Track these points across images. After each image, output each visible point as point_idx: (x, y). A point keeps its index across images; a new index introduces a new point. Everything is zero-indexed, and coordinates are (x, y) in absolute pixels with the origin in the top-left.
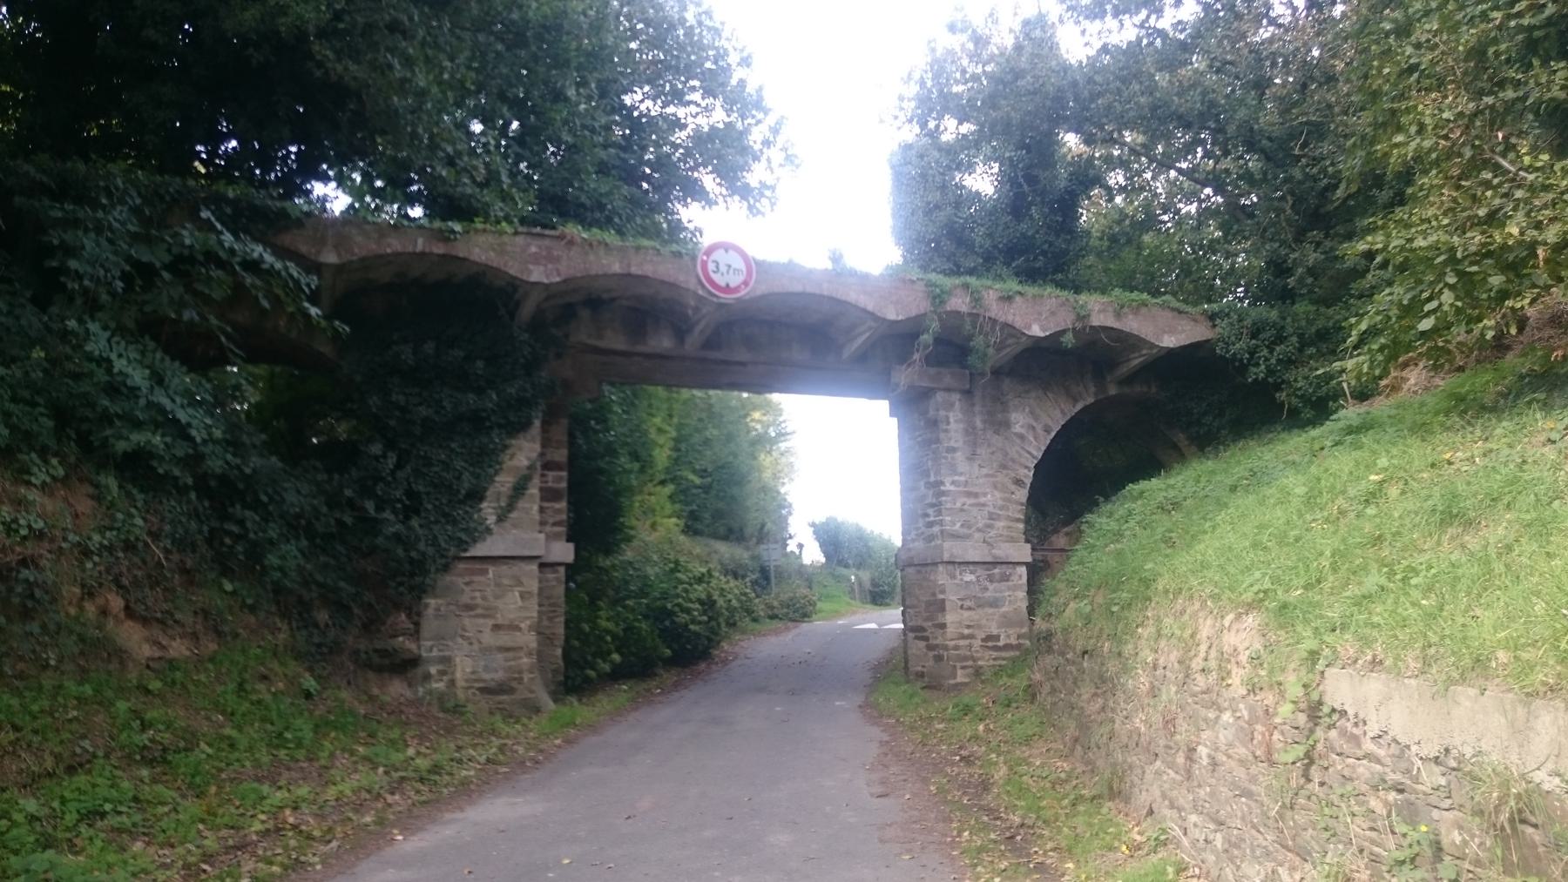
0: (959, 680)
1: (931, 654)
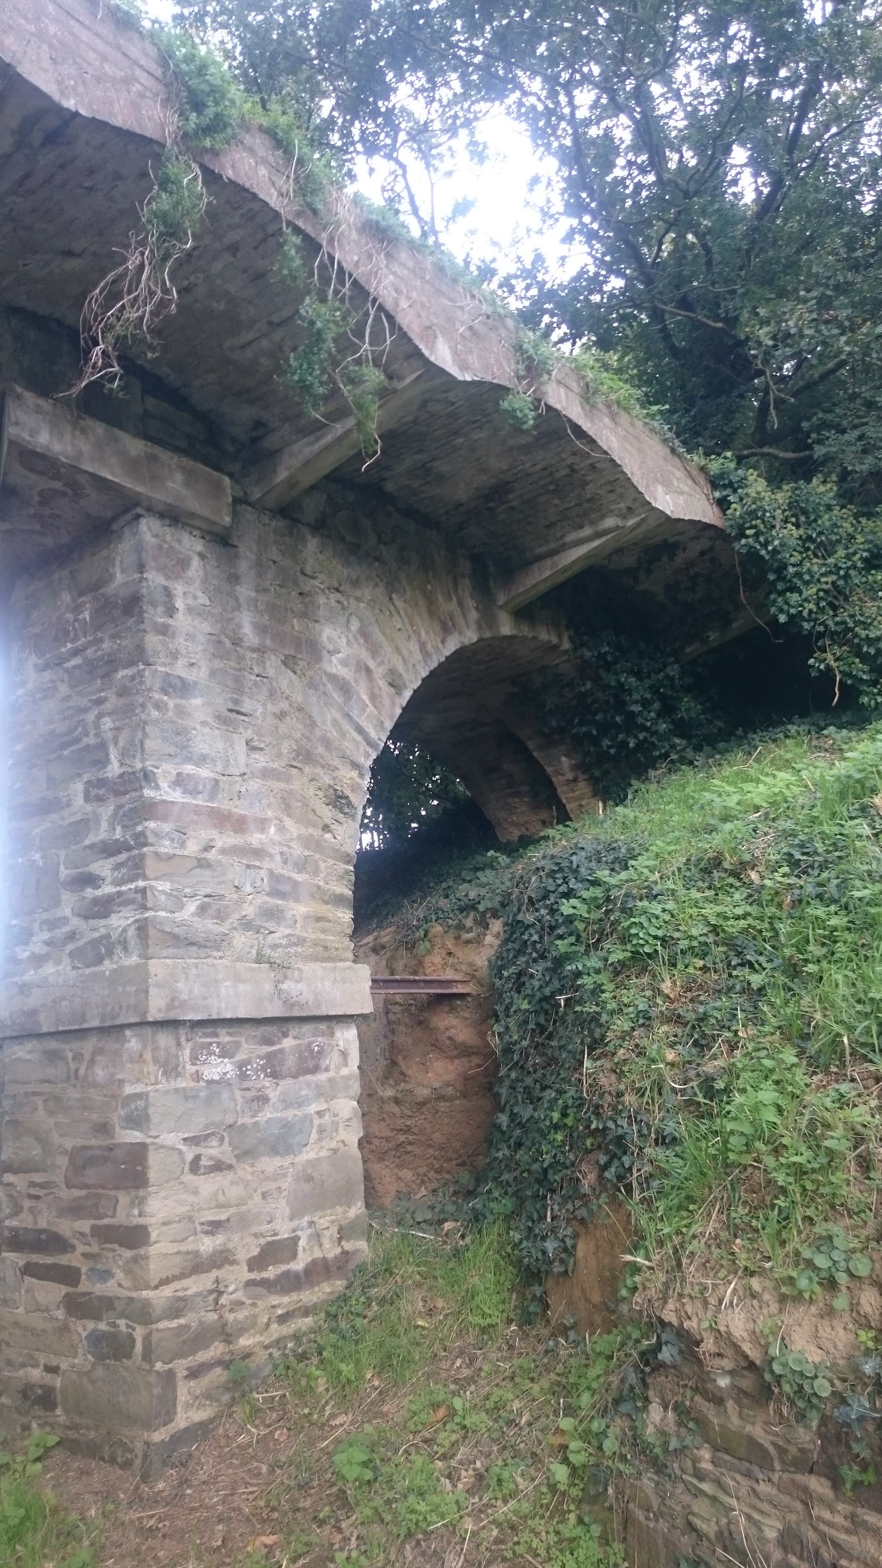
0: (183, 1419)
1: (83, 1328)
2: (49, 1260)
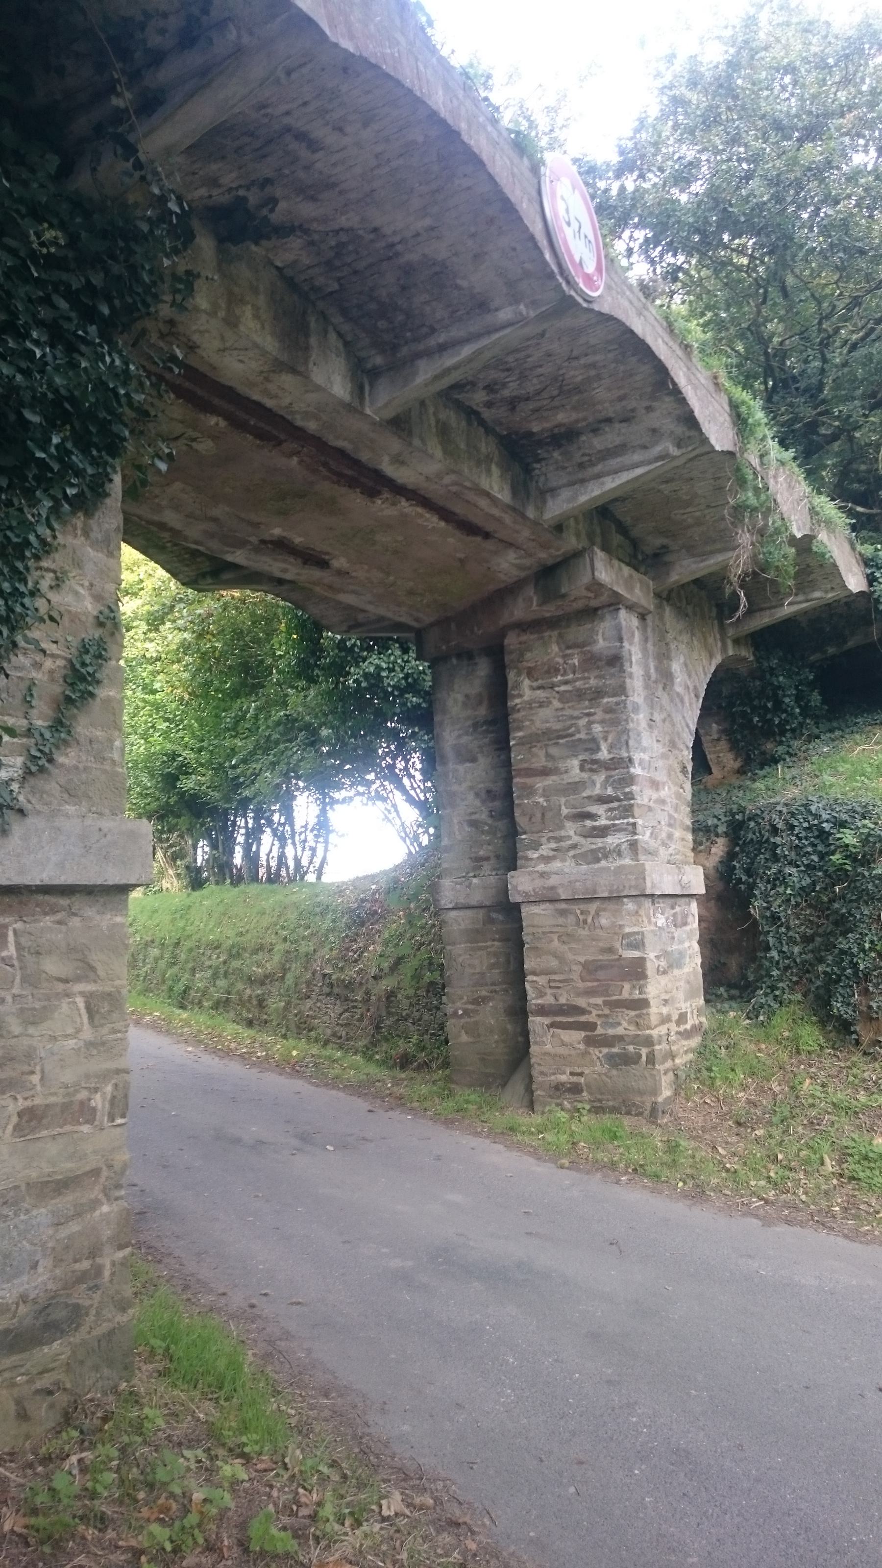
2: (571, 1020)
